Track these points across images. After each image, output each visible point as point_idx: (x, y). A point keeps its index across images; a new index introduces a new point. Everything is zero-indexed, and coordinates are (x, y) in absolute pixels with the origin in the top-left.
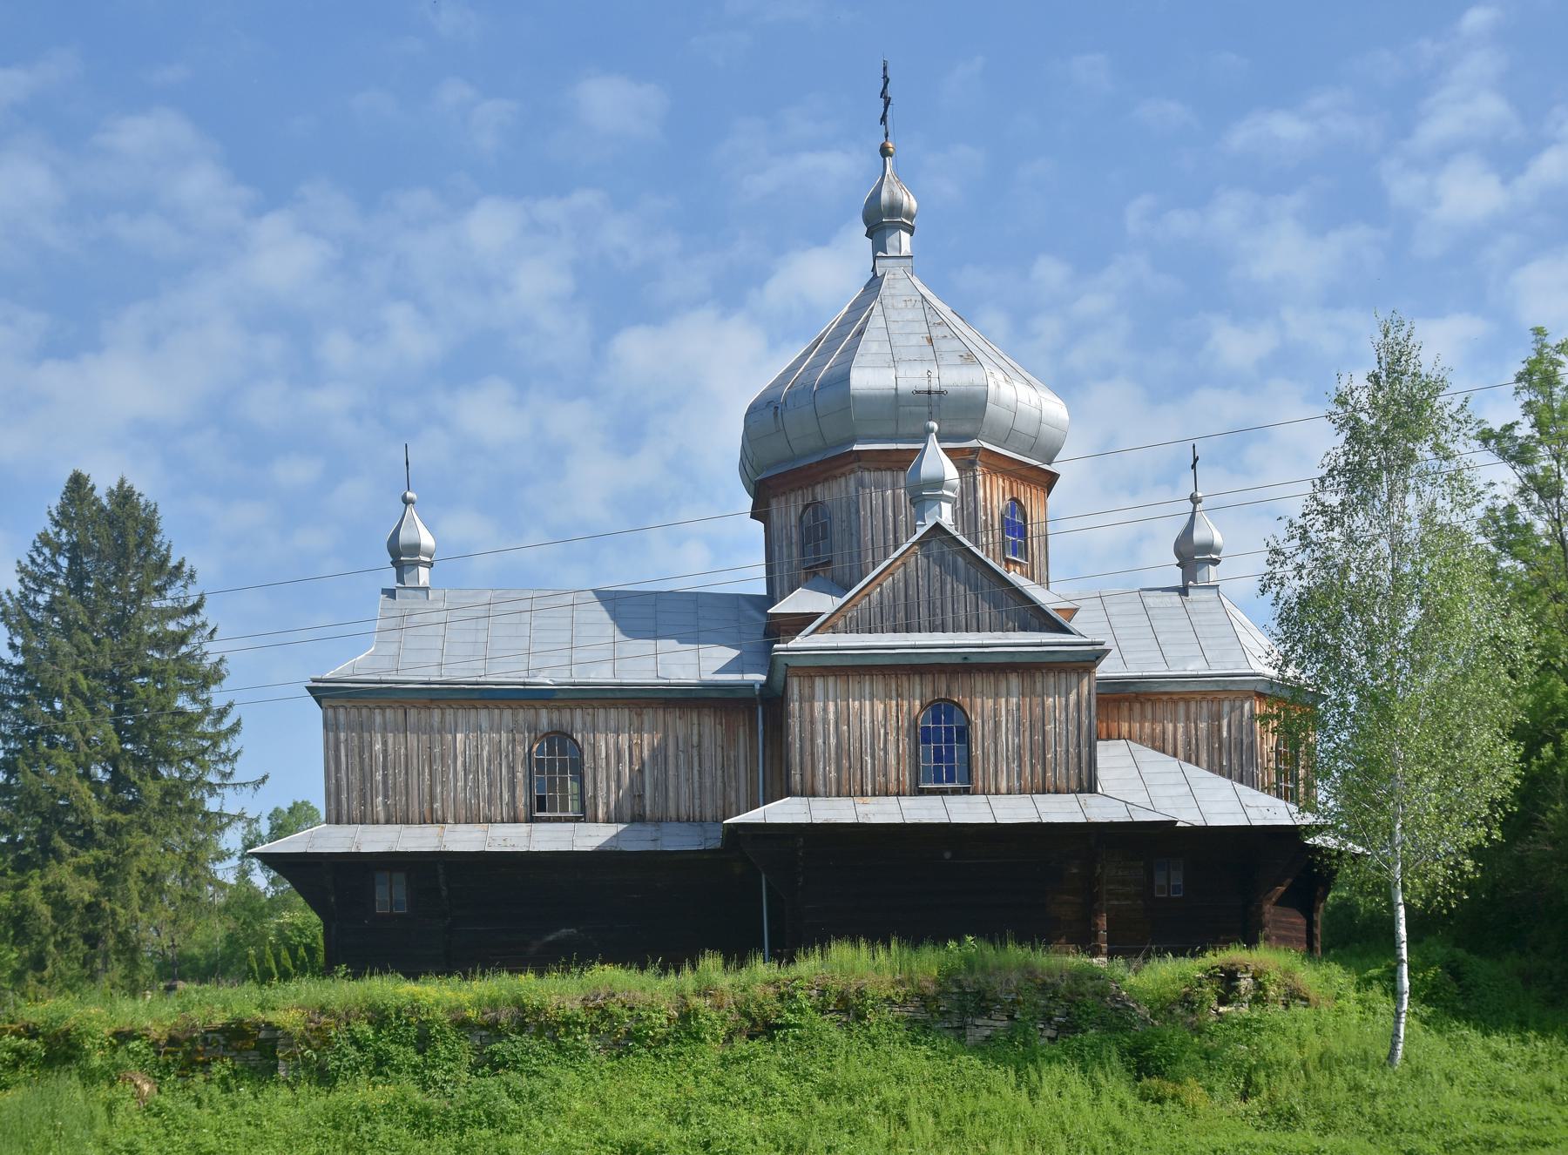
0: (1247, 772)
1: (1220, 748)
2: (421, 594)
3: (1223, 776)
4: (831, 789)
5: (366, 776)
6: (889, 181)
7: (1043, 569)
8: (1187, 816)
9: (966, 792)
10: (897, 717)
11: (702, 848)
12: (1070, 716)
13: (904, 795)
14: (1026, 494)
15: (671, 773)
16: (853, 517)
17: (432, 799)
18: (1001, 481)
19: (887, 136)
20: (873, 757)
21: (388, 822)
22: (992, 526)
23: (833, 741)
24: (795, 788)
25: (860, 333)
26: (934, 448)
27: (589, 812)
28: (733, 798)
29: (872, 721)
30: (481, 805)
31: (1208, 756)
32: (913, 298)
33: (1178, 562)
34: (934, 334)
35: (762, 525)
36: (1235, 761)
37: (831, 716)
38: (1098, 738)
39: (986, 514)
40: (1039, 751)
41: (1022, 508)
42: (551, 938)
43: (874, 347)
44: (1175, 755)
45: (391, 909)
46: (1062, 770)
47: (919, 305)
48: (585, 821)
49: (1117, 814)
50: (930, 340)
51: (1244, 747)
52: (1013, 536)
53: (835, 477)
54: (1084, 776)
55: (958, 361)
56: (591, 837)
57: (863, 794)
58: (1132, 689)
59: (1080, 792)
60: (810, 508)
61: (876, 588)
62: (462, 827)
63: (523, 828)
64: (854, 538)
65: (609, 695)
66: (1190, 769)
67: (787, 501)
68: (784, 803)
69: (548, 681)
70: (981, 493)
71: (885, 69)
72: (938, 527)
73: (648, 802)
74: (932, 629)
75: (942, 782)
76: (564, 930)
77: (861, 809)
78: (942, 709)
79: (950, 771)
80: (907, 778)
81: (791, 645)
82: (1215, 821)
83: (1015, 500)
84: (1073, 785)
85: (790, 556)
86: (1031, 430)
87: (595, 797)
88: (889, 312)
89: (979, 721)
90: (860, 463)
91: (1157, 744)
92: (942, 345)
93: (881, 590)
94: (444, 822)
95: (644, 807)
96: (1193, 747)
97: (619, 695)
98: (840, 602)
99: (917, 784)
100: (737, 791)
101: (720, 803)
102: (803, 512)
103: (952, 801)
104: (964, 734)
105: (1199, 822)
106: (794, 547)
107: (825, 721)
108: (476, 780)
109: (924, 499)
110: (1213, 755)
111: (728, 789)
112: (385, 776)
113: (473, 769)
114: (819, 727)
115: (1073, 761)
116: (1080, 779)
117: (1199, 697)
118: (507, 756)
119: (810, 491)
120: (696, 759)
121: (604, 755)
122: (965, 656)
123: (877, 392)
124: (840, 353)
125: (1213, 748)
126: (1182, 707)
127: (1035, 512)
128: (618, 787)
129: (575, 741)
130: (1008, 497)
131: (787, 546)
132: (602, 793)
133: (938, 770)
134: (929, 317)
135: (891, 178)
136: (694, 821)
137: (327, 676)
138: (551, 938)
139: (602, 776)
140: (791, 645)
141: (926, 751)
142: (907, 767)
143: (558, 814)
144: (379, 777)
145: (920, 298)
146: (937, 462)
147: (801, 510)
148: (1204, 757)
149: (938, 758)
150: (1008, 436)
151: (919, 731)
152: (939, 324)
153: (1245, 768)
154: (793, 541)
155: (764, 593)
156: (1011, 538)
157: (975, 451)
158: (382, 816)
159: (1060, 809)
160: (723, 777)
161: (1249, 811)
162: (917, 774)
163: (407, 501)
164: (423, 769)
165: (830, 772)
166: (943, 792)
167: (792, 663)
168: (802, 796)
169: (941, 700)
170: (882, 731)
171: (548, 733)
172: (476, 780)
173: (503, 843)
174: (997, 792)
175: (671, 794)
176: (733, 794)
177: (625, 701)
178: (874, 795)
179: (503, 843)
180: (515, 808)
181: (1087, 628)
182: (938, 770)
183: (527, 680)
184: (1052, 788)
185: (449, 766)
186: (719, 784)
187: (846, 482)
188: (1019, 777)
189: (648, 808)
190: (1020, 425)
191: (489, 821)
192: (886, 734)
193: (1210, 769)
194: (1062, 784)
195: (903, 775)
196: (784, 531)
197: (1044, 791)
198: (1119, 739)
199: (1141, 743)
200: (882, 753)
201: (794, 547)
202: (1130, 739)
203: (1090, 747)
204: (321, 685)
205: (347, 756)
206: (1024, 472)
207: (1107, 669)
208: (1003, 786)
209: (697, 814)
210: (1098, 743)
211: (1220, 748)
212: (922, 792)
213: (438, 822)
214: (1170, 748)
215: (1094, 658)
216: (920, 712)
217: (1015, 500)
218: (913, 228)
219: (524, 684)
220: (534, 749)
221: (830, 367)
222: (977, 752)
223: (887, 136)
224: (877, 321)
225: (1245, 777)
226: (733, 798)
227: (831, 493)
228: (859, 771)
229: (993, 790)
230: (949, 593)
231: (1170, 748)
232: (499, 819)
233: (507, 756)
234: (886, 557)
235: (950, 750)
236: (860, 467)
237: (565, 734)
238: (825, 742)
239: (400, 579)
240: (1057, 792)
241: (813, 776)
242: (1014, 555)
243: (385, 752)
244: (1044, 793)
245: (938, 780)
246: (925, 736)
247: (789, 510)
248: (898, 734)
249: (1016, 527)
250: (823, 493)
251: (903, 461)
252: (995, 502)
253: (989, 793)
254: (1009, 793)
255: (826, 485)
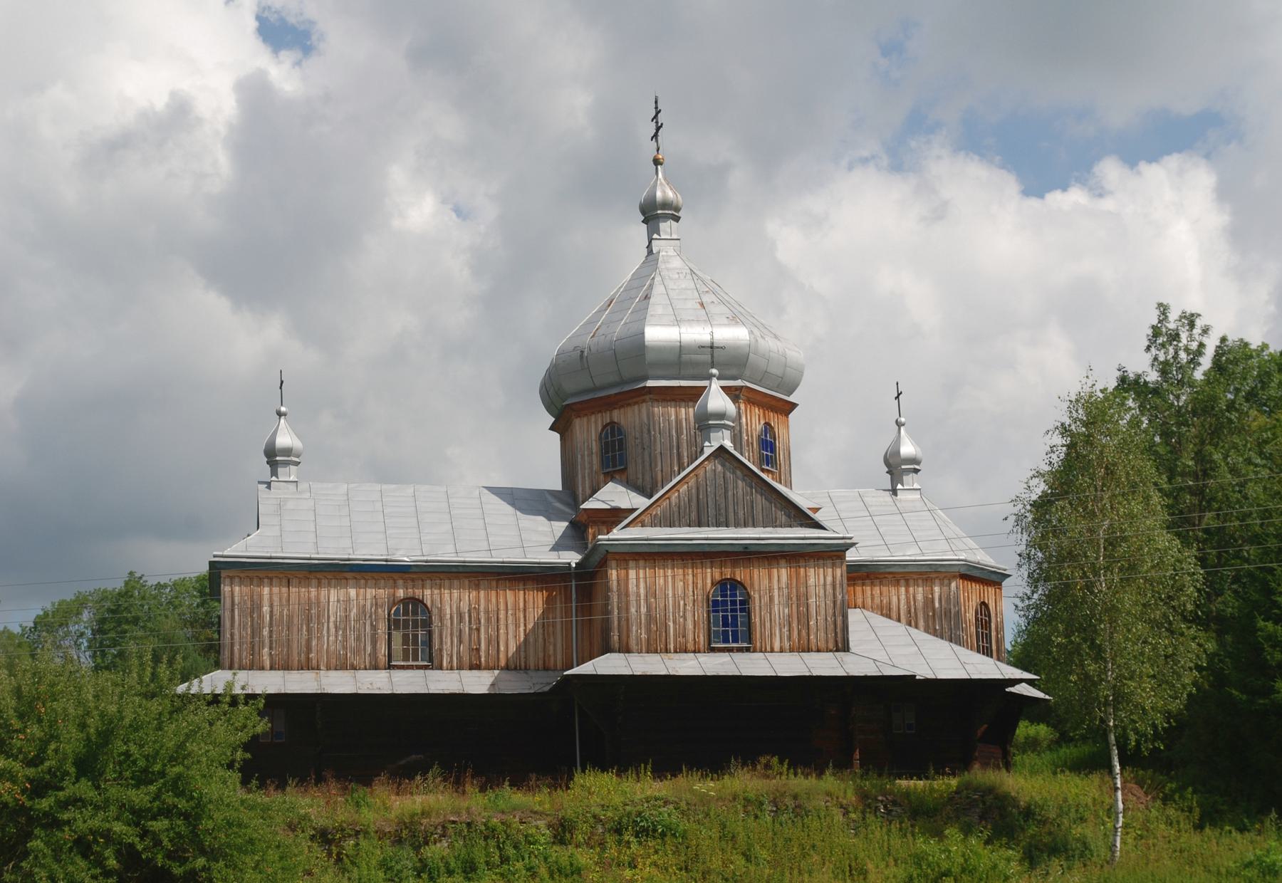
0: (955, 634)
1: (934, 615)
2: (292, 487)
3: (937, 636)
4: (641, 647)
5: (256, 631)
6: (661, 184)
7: (788, 475)
8: (923, 672)
9: (748, 650)
10: (693, 592)
11: (532, 691)
12: (827, 593)
13: (699, 652)
14: (774, 419)
15: (502, 631)
16: (645, 435)
17: (309, 649)
18: (757, 410)
19: (658, 150)
20: (674, 622)
21: (272, 668)
22: (752, 444)
23: (643, 610)
24: (614, 645)
25: (647, 297)
26: (715, 385)
27: (436, 662)
28: (551, 652)
29: (674, 595)
30: (349, 655)
31: (924, 622)
32: (684, 271)
33: (887, 470)
34: (704, 300)
35: (558, 436)
36: (945, 626)
37: (642, 591)
38: (849, 608)
39: (747, 435)
40: (804, 619)
41: (772, 428)
42: (403, 762)
43: (660, 310)
44: (899, 620)
45: (272, 739)
46: (822, 635)
47: (689, 276)
48: (432, 669)
49: (867, 670)
50: (702, 305)
51: (952, 616)
52: (767, 451)
53: (629, 405)
54: (839, 639)
55: (726, 321)
56: (478, 683)
57: (667, 651)
58: (865, 569)
59: (837, 650)
60: (609, 427)
61: (674, 493)
62: (333, 673)
63: (383, 674)
64: (646, 453)
65: (454, 570)
66: (913, 631)
67: (589, 421)
68: (607, 658)
69: (406, 559)
70: (744, 420)
71: (656, 102)
72: (722, 449)
73: (483, 654)
74: (718, 525)
75: (728, 642)
76: (414, 756)
77: (668, 663)
78: (728, 586)
79: (735, 634)
80: (702, 639)
81: (611, 536)
82: (943, 675)
83: (767, 424)
84: (831, 646)
85: (591, 463)
86: (779, 373)
87: (441, 650)
88: (667, 282)
89: (757, 596)
90: (651, 396)
91: (884, 612)
92: (713, 309)
93: (679, 495)
94: (318, 669)
95: (480, 658)
96: (913, 615)
97: (461, 570)
98: (647, 502)
99: (709, 644)
100: (555, 645)
101: (541, 655)
102: (602, 430)
103: (738, 657)
104: (746, 604)
105: (930, 676)
106: (594, 456)
107: (638, 595)
108: (345, 636)
109: (710, 427)
110: (928, 621)
111: (547, 644)
112: (271, 632)
113: (342, 626)
114: (632, 598)
115: (831, 627)
116: (836, 642)
117: (915, 577)
118: (371, 616)
119: (608, 415)
120: (522, 620)
121: (448, 616)
122: (746, 546)
123: (665, 344)
124: (632, 313)
125: (928, 615)
126: (902, 582)
127: (780, 431)
128: (460, 642)
129: (426, 606)
130: (762, 422)
131: (588, 456)
132: (447, 646)
133: (725, 633)
134: (698, 286)
135: (663, 181)
136: (520, 669)
137: (226, 553)
138: (403, 762)
139: (447, 633)
140: (611, 536)
141: (716, 619)
142: (702, 631)
143: (411, 663)
144: (266, 632)
145: (689, 271)
146: (717, 400)
147: (600, 429)
148: (921, 623)
149: (725, 624)
150: (763, 377)
151: (711, 603)
152: (707, 292)
153: (953, 632)
154: (594, 451)
155: (557, 484)
156: (765, 453)
157: (740, 388)
158: (267, 664)
159: (823, 665)
160: (544, 634)
161: (966, 666)
162: (709, 636)
163: (280, 414)
164: (302, 627)
165: (641, 634)
166: (730, 650)
167: (611, 550)
168: (619, 652)
169: (728, 579)
170: (682, 603)
171: (404, 599)
172: (345, 636)
173: (369, 686)
174: (772, 651)
175: (502, 648)
176: (551, 648)
177: (466, 575)
178: (676, 652)
179: (369, 686)
180: (376, 658)
181: (834, 528)
182: (725, 633)
183: (389, 557)
184: (814, 649)
185: (323, 624)
186: (541, 640)
187: (639, 411)
188: (790, 638)
189: (483, 659)
190: (772, 369)
191: (354, 668)
192: (685, 605)
193: (927, 630)
194: (822, 645)
195: (698, 637)
196: (586, 444)
197: (809, 650)
198: (855, 608)
199: (873, 611)
200: (681, 620)
201: (594, 456)
202: (864, 608)
203: (843, 616)
204: (222, 559)
205: (240, 616)
206: (773, 403)
207: (851, 556)
208: (777, 646)
209: (523, 664)
210: (849, 610)
211: (934, 615)
212: (713, 650)
213: (313, 669)
214: (894, 615)
215: (844, 548)
216: (711, 588)
217: (767, 424)
218: (680, 218)
219: (386, 561)
220: (393, 612)
221: (625, 323)
222: (756, 620)
223: (658, 150)
224: (658, 290)
225: (954, 639)
226: (551, 652)
227: (627, 417)
228: (664, 634)
229: (768, 649)
230: (730, 498)
231: (894, 615)
232: (363, 666)
233: (371, 616)
234: (681, 468)
235: (735, 618)
236: (650, 399)
237: (418, 600)
238: (637, 610)
239: (274, 473)
240: (818, 651)
241: (628, 637)
242: (768, 465)
243: (271, 612)
244: (809, 652)
245: (726, 641)
246: (714, 606)
247: (588, 430)
248: (694, 605)
249: (768, 446)
250: (617, 415)
251: (694, 395)
252: (754, 426)
253: (766, 651)
254: (781, 652)
255: (622, 410)
